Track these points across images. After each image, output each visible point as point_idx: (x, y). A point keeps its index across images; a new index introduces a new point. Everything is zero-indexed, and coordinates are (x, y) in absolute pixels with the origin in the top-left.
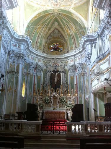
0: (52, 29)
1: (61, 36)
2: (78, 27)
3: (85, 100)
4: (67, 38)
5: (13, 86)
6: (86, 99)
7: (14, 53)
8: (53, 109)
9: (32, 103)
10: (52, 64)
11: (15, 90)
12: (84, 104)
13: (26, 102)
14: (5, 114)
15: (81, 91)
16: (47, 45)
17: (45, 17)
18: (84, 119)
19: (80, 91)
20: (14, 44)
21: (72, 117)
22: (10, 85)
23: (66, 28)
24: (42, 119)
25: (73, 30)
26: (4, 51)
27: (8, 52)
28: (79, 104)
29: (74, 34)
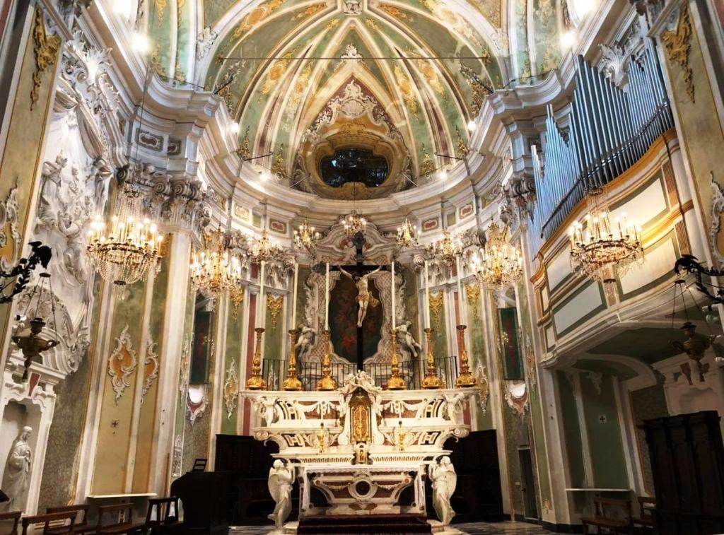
0: (335, 82)
1: (375, 114)
2: (456, 66)
3: (507, 411)
4: (403, 123)
5: (137, 343)
6: (511, 403)
7: (148, 177)
8: (354, 462)
9: (239, 432)
10: (338, 242)
11: (150, 365)
12: (501, 434)
13: (209, 428)
14: (88, 494)
15: (484, 362)
16: (309, 153)
17: (299, 21)
18: (507, 506)
19: (480, 365)
20: (148, 136)
21: (454, 501)
22: (124, 337)
23: (399, 75)
24: (292, 516)
25: (434, 81)
26: (91, 161)
27: (112, 169)
28: (475, 429)
29: (437, 103)
